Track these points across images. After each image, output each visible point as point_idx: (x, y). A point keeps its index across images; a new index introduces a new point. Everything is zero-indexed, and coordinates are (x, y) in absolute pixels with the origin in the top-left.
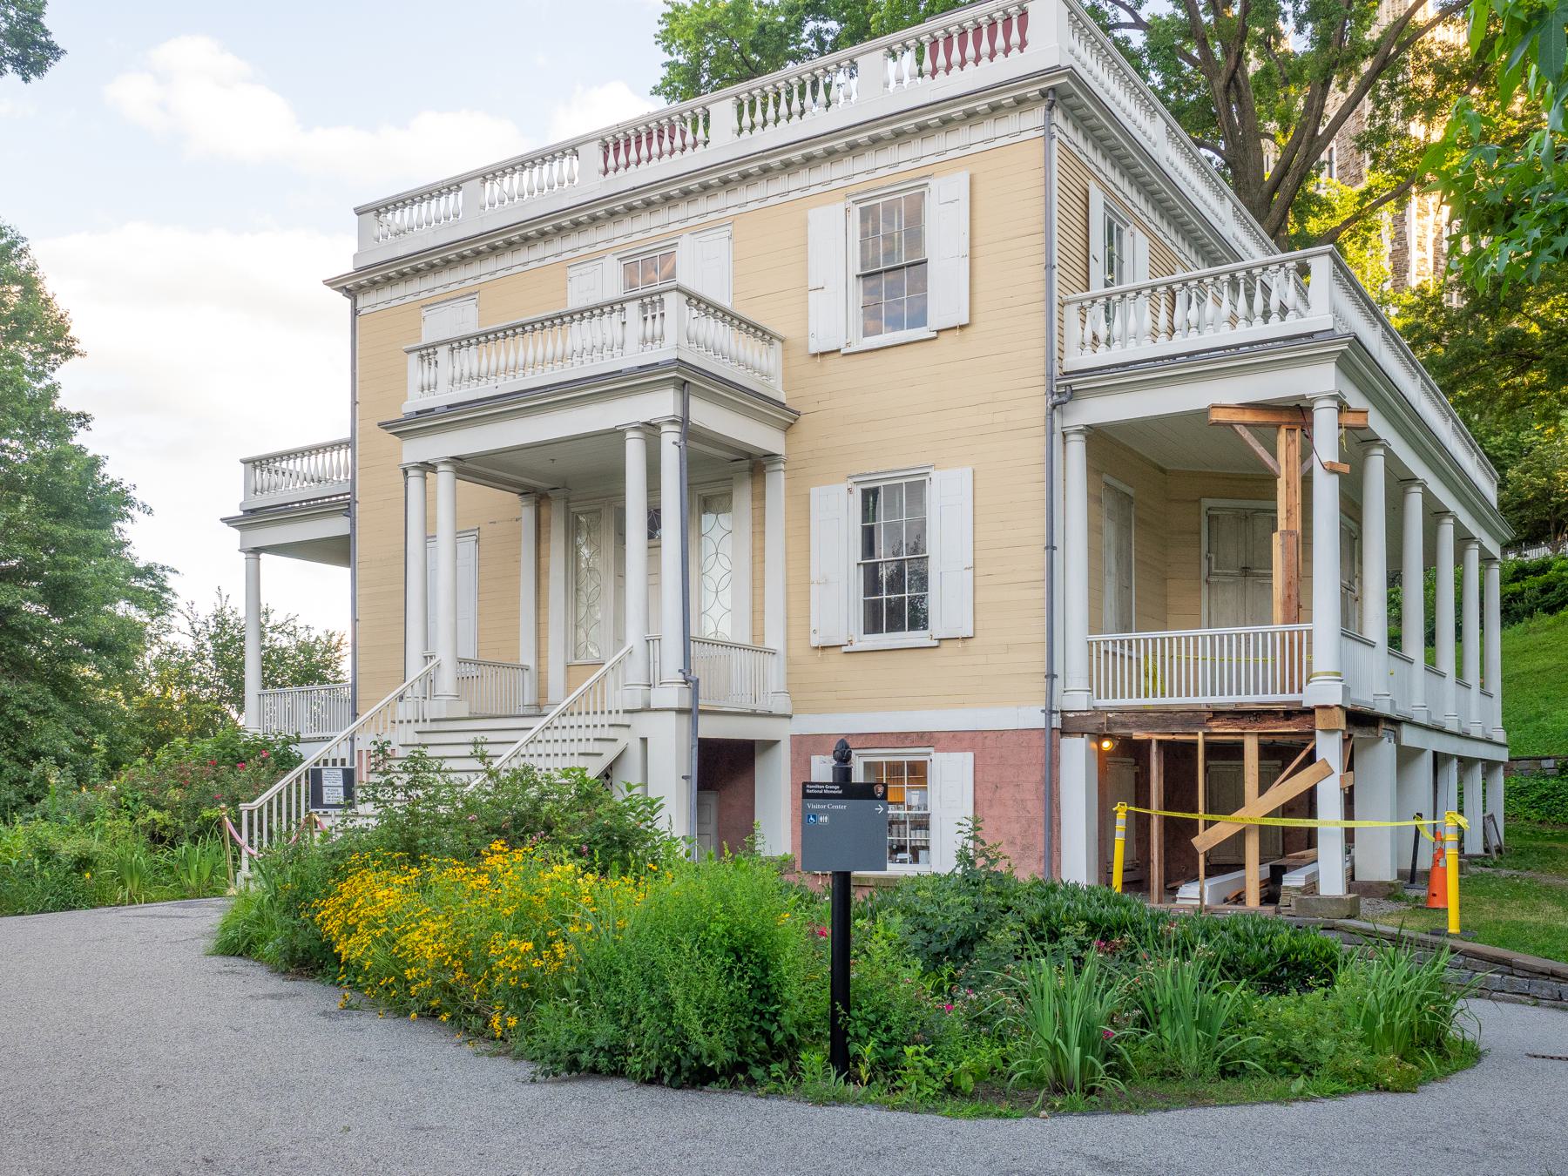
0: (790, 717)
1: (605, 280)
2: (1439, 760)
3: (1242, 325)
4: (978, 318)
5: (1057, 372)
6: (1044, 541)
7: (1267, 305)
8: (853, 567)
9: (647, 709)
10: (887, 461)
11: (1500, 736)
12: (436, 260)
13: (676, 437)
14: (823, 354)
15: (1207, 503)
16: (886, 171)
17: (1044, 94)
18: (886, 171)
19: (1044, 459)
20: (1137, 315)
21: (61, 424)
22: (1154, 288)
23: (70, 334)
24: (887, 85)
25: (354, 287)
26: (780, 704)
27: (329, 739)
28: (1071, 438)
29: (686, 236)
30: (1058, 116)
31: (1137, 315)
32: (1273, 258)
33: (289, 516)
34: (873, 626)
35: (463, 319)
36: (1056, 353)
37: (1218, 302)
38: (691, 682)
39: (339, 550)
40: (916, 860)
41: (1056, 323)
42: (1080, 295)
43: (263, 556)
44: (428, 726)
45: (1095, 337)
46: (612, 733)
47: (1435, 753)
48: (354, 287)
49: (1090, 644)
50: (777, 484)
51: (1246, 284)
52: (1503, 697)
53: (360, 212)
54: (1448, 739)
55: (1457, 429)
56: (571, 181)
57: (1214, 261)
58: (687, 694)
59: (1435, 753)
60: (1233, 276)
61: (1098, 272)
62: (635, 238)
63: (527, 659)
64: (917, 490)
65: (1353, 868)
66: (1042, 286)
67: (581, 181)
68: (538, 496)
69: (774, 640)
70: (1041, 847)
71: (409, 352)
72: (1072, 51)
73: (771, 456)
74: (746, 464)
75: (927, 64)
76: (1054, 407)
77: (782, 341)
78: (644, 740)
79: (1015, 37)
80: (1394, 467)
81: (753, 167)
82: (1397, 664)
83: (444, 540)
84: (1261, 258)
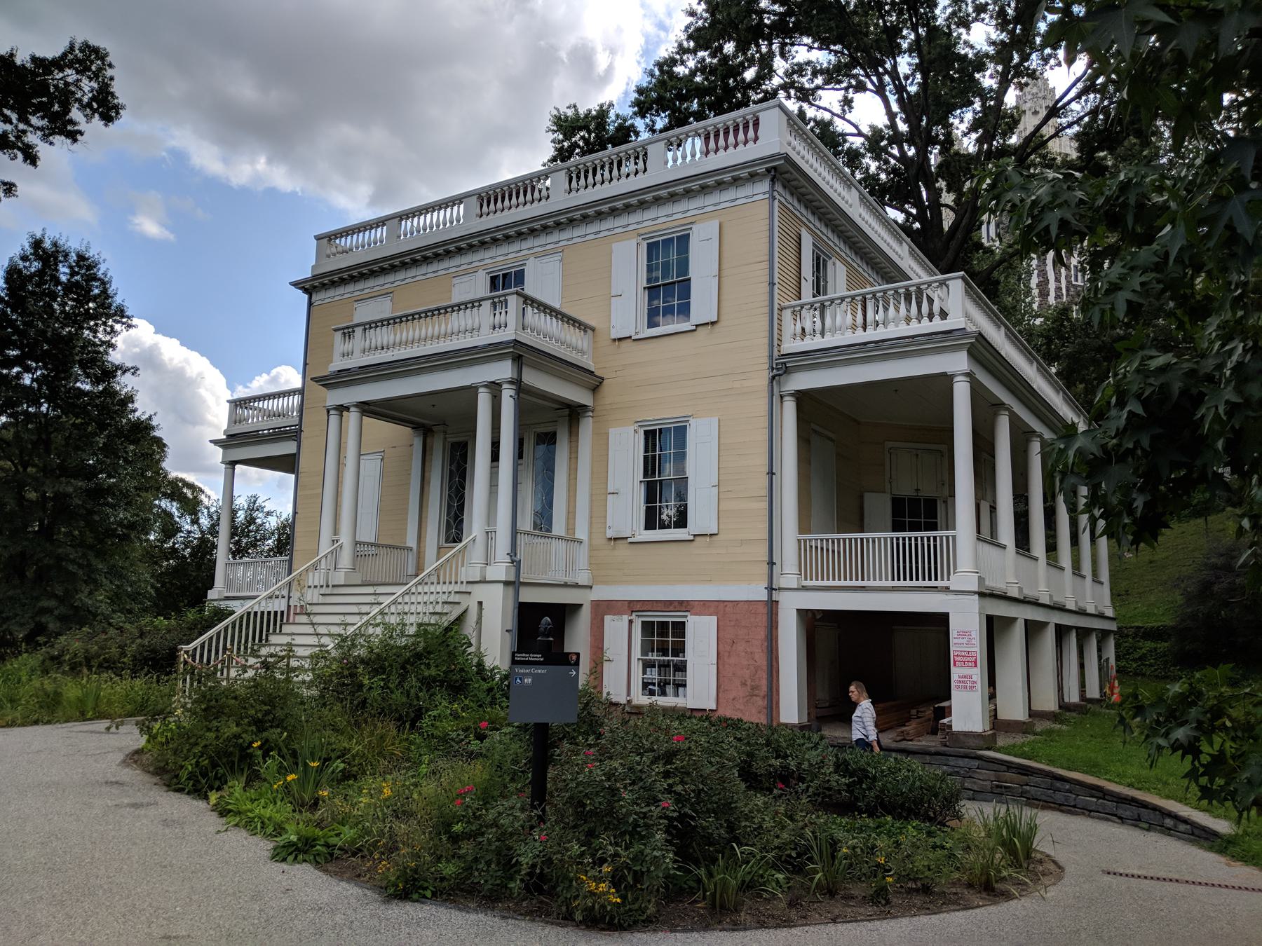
1: (479, 286)
2: (1061, 632)
3: (914, 324)
4: (722, 318)
5: (776, 354)
6: (766, 469)
7: (931, 309)
9: (483, 582)
10: (662, 413)
11: (1109, 612)
12: (365, 271)
13: (512, 393)
14: (620, 339)
15: (889, 444)
16: (665, 219)
17: (768, 170)
18: (665, 219)
19: (767, 413)
20: (841, 316)
21: (109, 373)
22: (853, 298)
24: (666, 163)
25: (310, 287)
26: (583, 579)
27: (254, 598)
28: (786, 398)
29: (532, 259)
30: (779, 187)
31: (841, 316)
32: (935, 278)
33: (258, 440)
34: (650, 525)
35: (383, 309)
36: (776, 342)
37: (897, 310)
38: (516, 563)
39: (287, 464)
40: (676, 694)
41: (776, 321)
42: (793, 303)
43: (238, 467)
44: (329, 591)
45: (803, 329)
46: (457, 598)
47: (1026, 621)
48: (310, 287)
49: (799, 541)
50: (587, 427)
51: (915, 296)
52: (1111, 583)
53: (318, 238)
54: (1041, 610)
56: (381, 242)
57: (890, 280)
58: (513, 570)
59: (1026, 621)
60: (896, 292)
61: (807, 289)
62: (675, 217)
63: (411, 542)
64: (681, 432)
65: (996, 710)
66: (766, 297)
67: (456, 221)
68: (425, 430)
69: (582, 533)
70: (764, 689)
71: (336, 330)
72: (789, 144)
74: (567, 412)
75: (712, 144)
76: (773, 377)
77: (593, 330)
78: (480, 603)
79: (751, 133)
80: (1015, 423)
81: (537, 225)
82: (1024, 561)
83: (365, 462)
84: (926, 278)
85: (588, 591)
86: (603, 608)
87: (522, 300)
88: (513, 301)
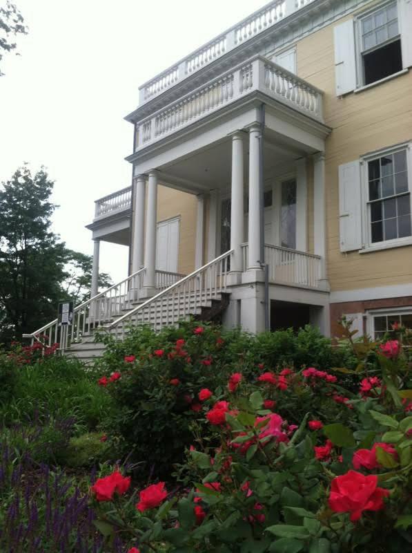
0: (329, 293)
8: (364, 205)
9: (240, 285)
23: (49, 231)
26: (324, 286)
48: (134, 118)
50: (321, 169)
55: (298, 436)
69: (319, 250)
73: (318, 152)
85: (347, 217)
86: (340, 309)
87: (263, 64)
88: (256, 66)
